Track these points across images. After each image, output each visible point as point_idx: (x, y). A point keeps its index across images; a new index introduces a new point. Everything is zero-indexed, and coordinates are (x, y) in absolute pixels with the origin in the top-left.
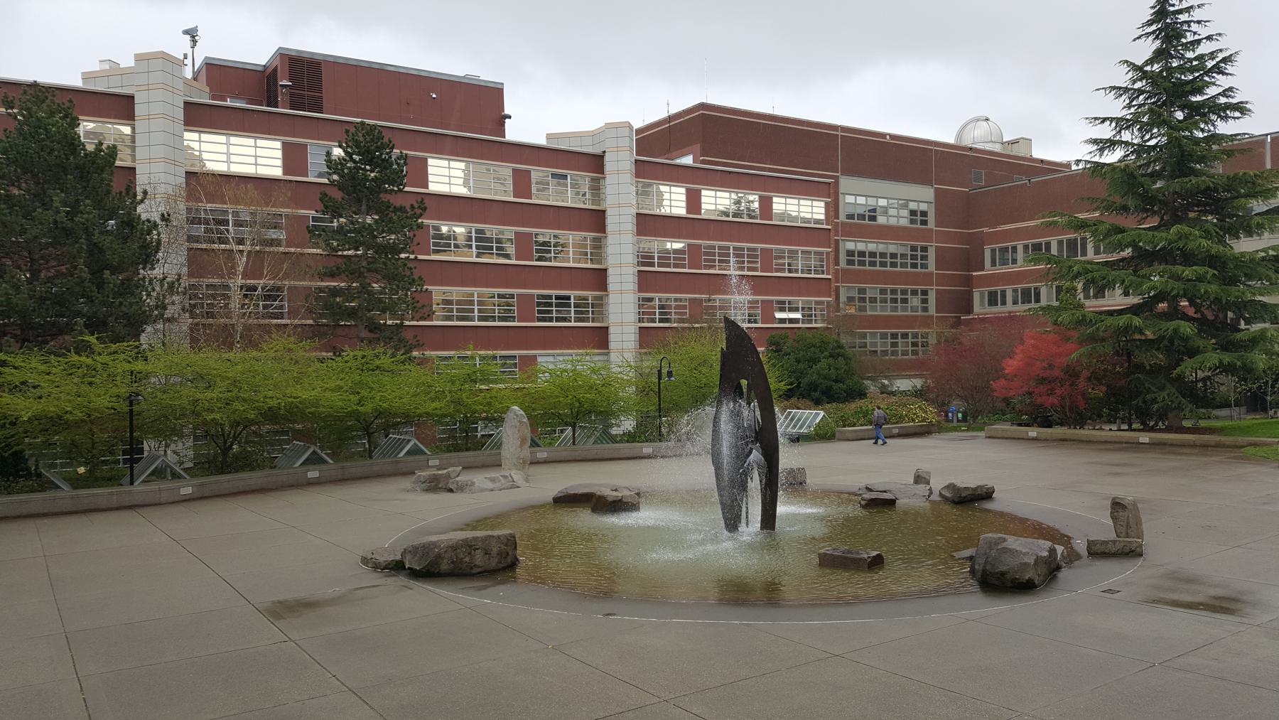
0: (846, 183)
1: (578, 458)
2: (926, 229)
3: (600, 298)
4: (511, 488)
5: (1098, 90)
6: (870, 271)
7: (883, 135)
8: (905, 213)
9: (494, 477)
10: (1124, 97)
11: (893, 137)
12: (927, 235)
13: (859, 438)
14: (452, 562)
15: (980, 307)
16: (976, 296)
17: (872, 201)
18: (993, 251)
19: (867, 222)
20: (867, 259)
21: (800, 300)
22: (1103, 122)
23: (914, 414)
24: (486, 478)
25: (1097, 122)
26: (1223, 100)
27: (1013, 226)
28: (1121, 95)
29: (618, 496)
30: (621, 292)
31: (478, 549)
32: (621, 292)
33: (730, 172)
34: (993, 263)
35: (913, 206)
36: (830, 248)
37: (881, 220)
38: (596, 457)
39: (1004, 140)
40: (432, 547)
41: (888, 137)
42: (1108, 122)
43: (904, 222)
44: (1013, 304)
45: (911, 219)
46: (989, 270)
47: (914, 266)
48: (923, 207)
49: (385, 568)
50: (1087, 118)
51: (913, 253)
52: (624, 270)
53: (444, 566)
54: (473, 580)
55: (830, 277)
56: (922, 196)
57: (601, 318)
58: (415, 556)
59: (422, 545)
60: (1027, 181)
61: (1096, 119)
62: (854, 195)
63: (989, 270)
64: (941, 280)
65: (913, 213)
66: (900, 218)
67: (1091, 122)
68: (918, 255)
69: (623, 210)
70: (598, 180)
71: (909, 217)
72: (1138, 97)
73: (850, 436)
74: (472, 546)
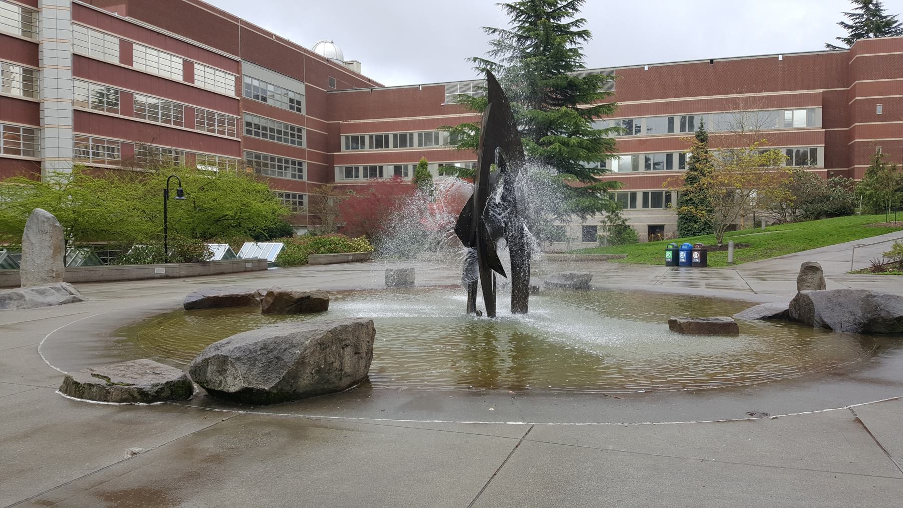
0: (246, 67)
1: (80, 280)
2: (300, 115)
3: (31, 131)
4: (73, 302)
5: (498, 4)
6: (262, 141)
7: (271, 35)
8: (287, 100)
9: (44, 290)
10: (512, 14)
11: (278, 38)
12: (300, 120)
13: (329, 262)
14: (319, 371)
15: (339, 177)
16: (337, 170)
17: (263, 86)
18: (347, 138)
19: (260, 101)
20: (261, 131)
21: (217, 156)
22: (494, 32)
23: (359, 245)
24: (32, 290)
25: (491, 31)
26: (574, 29)
27: (362, 121)
28: (511, 12)
29: (305, 292)
30: (58, 127)
31: (347, 346)
32: (58, 127)
33: (158, 33)
34: (347, 148)
35: (291, 95)
36: (239, 116)
37: (270, 102)
38: (101, 278)
39: (345, 60)
40: (283, 346)
41: (274, 37)
42: (498, 33)
43: (286, 107)
44: (364, 177)
45: (290, 105)
46: (344, 151)
47: (293, 142)
48: (297, 98)
49: (156, 398)
50: (484, 27)
51: (286, 130)
52: (62, 105)
53: (306, 381)
54: (283, 406)
55: (239, 140)
56: (297, 88)
57: (31, 152)
58: (254, 365)
59: (261, 345)
60: (370, 90)
61: (490, 28)
62: (251, 77)
63: (344, 151)
64: (311, 156)
65: (292, 101)
66: (279, 102)
67: (486, 31)
68: (296, 133)
69: (61, 46)
70: (30, 12)
71: (289, 103)
72: (521, 16)
73: (323, 261)
74: (342, 340)
